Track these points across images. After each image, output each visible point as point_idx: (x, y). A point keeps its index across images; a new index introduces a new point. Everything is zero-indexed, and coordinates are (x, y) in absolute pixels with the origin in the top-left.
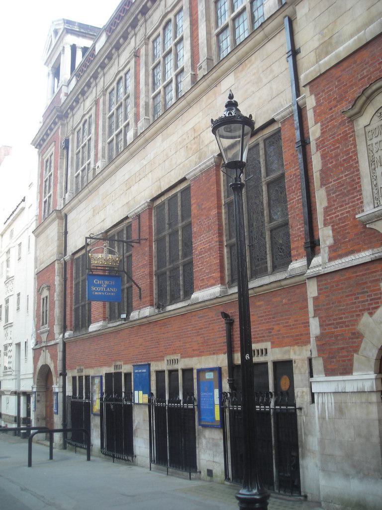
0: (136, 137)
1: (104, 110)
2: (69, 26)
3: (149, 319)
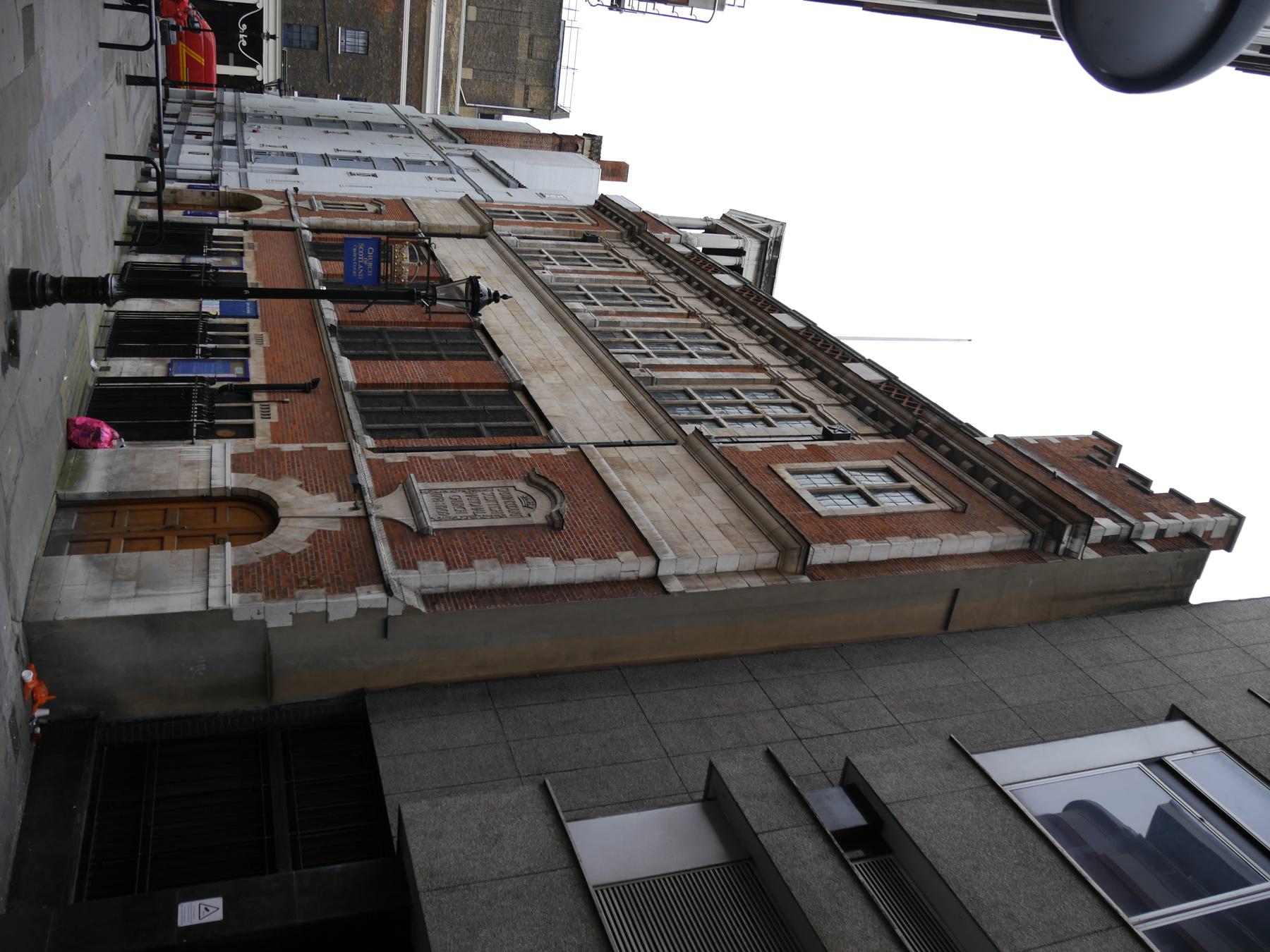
0: (625, 367)
1: (628, 282)
2: (771, 245)
3: (320, 318)
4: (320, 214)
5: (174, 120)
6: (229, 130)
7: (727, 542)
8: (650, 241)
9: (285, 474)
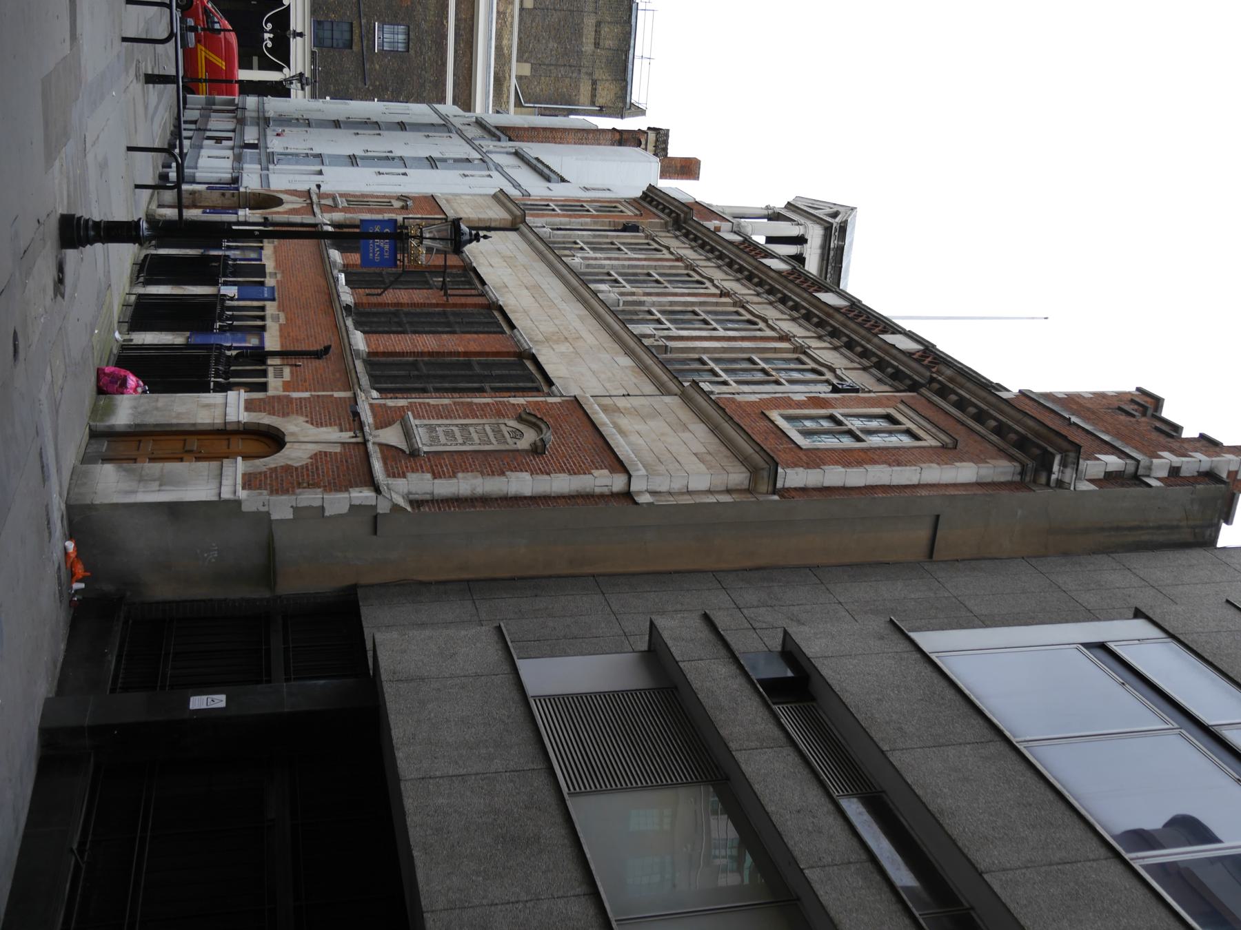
0: (639, 338)
1: (663, 267)
4: (344, 210)
5: (193, 126)
6: (251, 135)
7: (702, 465)
8: (695, 229)
9: (293, 413)
